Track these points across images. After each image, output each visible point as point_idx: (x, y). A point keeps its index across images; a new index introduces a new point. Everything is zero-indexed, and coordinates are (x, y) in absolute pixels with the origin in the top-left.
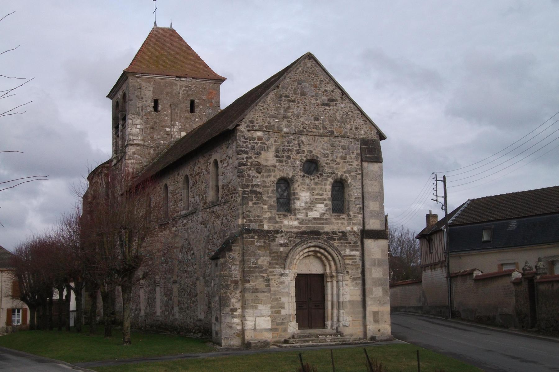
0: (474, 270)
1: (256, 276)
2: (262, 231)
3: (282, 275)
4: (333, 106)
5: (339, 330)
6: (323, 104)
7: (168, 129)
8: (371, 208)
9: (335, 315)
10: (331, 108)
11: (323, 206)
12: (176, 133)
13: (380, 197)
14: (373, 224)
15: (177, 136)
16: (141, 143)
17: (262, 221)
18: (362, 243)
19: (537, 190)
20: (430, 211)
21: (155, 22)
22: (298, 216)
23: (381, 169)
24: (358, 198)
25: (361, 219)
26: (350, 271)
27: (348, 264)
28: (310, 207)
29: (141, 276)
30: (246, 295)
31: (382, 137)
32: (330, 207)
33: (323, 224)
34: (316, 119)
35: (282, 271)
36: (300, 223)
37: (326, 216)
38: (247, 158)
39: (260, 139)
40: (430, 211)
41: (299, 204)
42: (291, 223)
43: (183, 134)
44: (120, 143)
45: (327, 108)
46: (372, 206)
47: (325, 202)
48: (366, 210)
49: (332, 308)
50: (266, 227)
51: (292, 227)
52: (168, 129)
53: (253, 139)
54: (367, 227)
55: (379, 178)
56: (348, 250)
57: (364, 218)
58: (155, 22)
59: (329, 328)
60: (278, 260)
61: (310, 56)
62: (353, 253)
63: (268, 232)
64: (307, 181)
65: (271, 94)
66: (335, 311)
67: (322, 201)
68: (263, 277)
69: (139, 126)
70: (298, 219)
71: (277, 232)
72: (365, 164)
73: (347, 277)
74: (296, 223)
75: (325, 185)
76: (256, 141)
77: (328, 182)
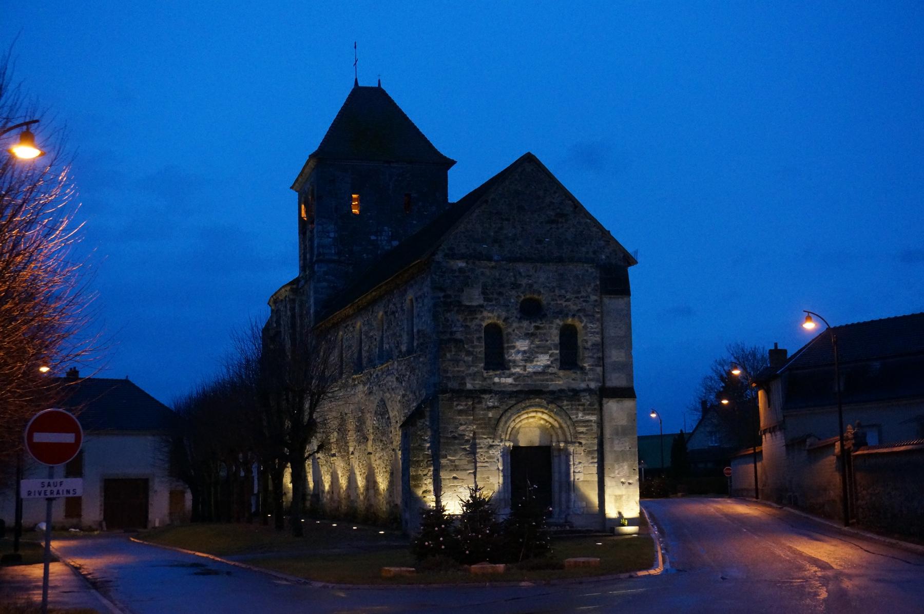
0: (809, 436)
1: (455, 450)
2: (463, 391)
3: (491, 446)
4: (562, 222)
5: (569, 519)
6: (552, 222)
7: (373, 238)
8: (614, 359)
9: (563, 499)
10: (560, 225)
11: (547, 357)
12: (384, 243)
13: (626, 342)
14: (616, 380)
15: (386, 248)
16: (336, 258)
17: (463, 378)
18: (601, 405)
19: (904, 318)
20: (776, 345)
21: (356, 80)
22: (513, 370)
23: (628, 304)
24: (598, 345)
25: (601, 374)
26: (583, 442)
27: (582, 433)
28: (529, 357)
29: (316, 448)
30: (441, 474)
31: (629, 260)
32: (558, 357)
33: (547, 380)
34: (539, 242)
35: (490, 441)
36: (515, 380)
37: (550, 370)
38: (444, 297)
39: (461, 270)
40: (776, 345)
41: (514, 356)
42: (503, 380)
43: (395, 243)
44: (308, 256)
45: (554, 226)
46: (615, 355)
47: (550, 352)
48: (607, 361)
49: (560, 492)
50: (469, 386)
51: (505, 385)
52: (373, 238)
53: (453, 271)
54: (609, 384)
55: (626, 316)
56: (580, 415)
57: (604, 372)
58: (356, 80)
59: (556, 516)
60: (485, 428)
61: (529, 159)
62: (587, 417)
63: (470, 391)
64: (525, 324)
65: (477, 211)
66: (564, 495)
67: (544, 350)
68: (465, 449)
69: (332, 235)
70: (513, 374)
71: (484, 391)
72: (606, 300)
73: (580, 450)
74: (510, 380)
75: (550, 328)
76: (457, 274)
77: (554, 326)
